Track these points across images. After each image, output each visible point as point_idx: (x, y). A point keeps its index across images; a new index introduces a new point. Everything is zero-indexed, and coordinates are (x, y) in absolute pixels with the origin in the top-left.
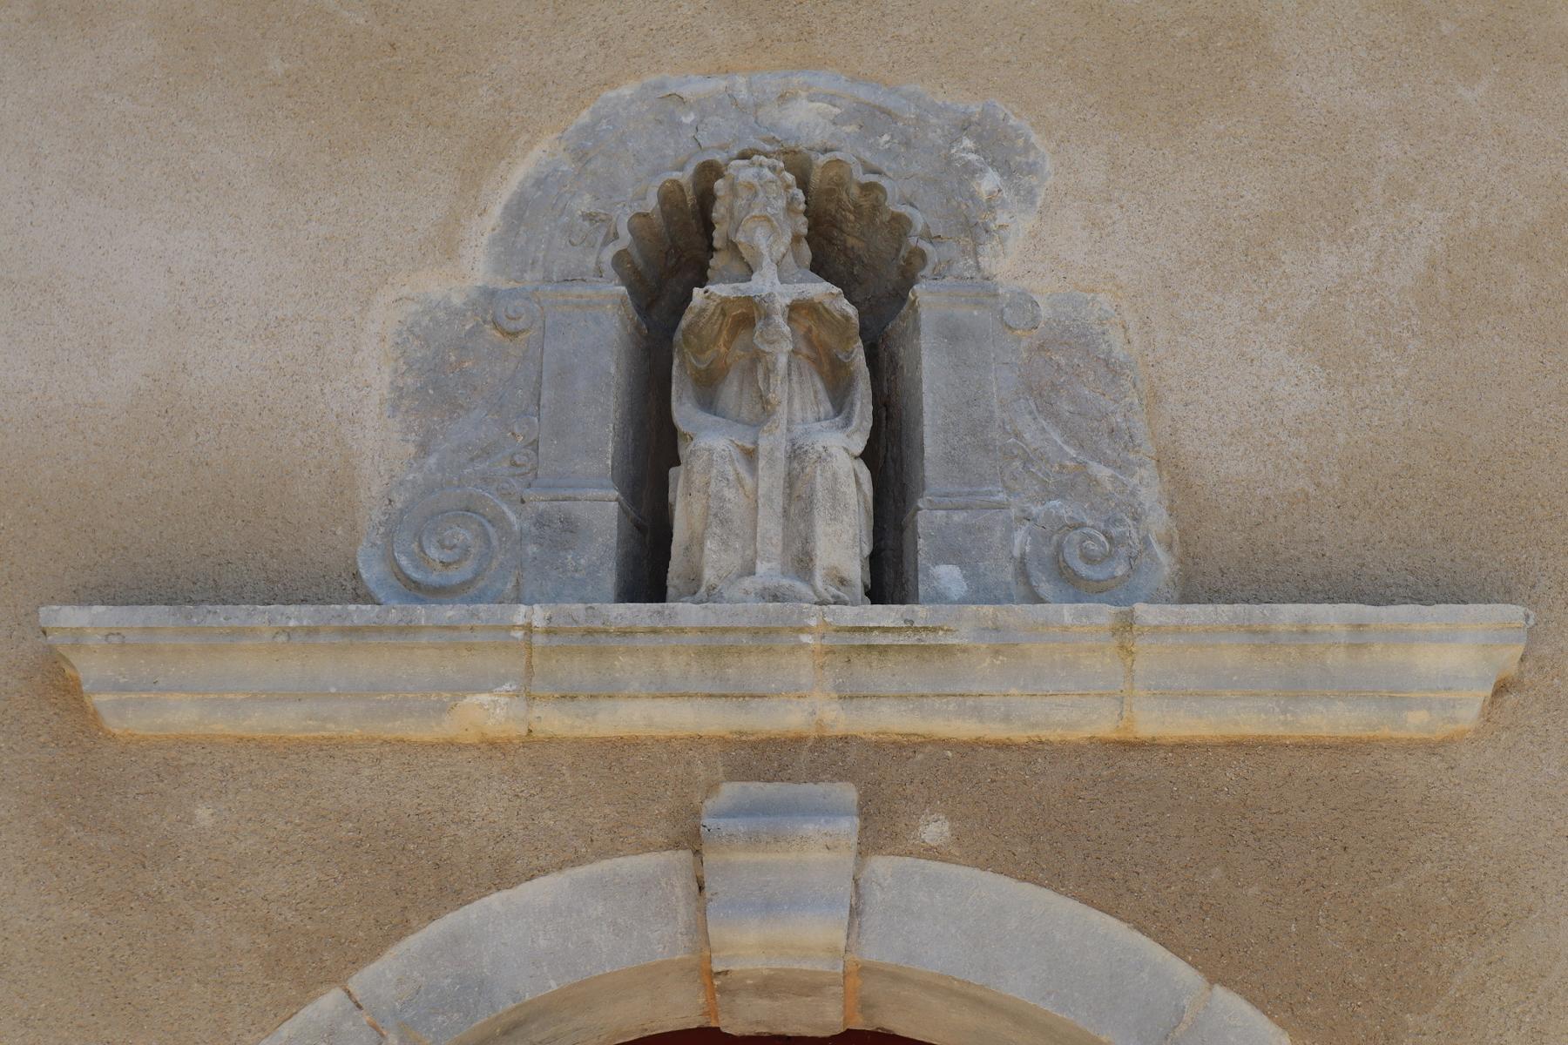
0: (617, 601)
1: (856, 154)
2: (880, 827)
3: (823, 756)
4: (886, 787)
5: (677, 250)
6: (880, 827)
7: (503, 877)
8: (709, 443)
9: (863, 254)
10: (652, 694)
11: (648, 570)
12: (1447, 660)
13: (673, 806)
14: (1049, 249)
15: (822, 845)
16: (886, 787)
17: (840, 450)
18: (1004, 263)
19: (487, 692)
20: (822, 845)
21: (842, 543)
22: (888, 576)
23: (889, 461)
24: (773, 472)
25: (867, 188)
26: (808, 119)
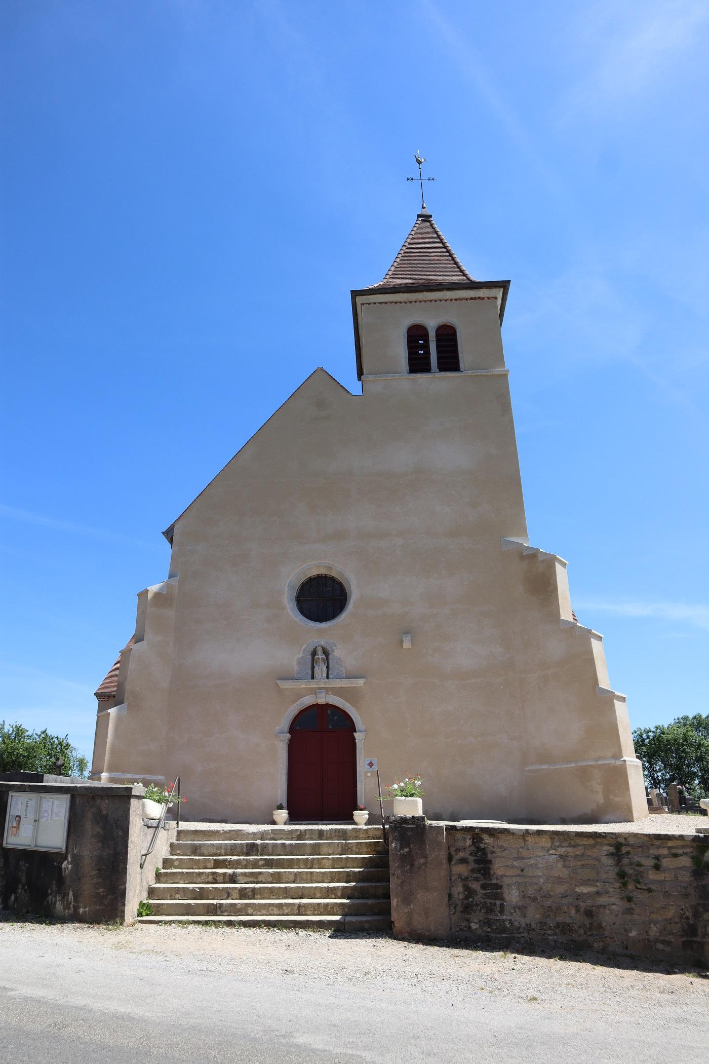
0: (340, 931)
1: (325, 646)
2: (327, 693)
3: (324, 688)
4: (327, 690)
5: (314, 653)
6: (327, 693)
7: (362, 810)
8: (316, 668)
9: (326, 652)
10: (313, 685)
11: (313, 678)
12: (361, 682)
13: (314, 691)
14: (337, 653)
15: (323, 695)
16: (327, 690)
17: (325, 668)
18: (335, 654)
19: (303, 685)
20: (323, 695)
21: (325, 675)
22: (328, 678)
23: (328, 668)
24: (321, 670)
25: (265, 1032)
26: (322, 643)
